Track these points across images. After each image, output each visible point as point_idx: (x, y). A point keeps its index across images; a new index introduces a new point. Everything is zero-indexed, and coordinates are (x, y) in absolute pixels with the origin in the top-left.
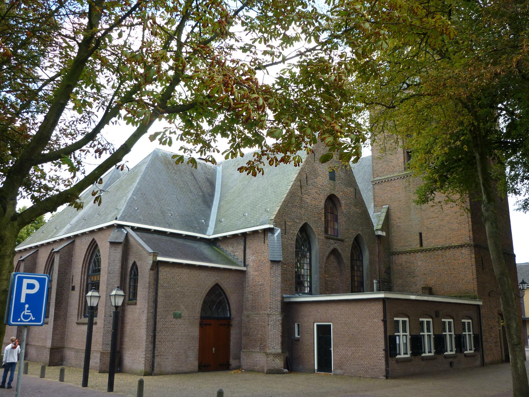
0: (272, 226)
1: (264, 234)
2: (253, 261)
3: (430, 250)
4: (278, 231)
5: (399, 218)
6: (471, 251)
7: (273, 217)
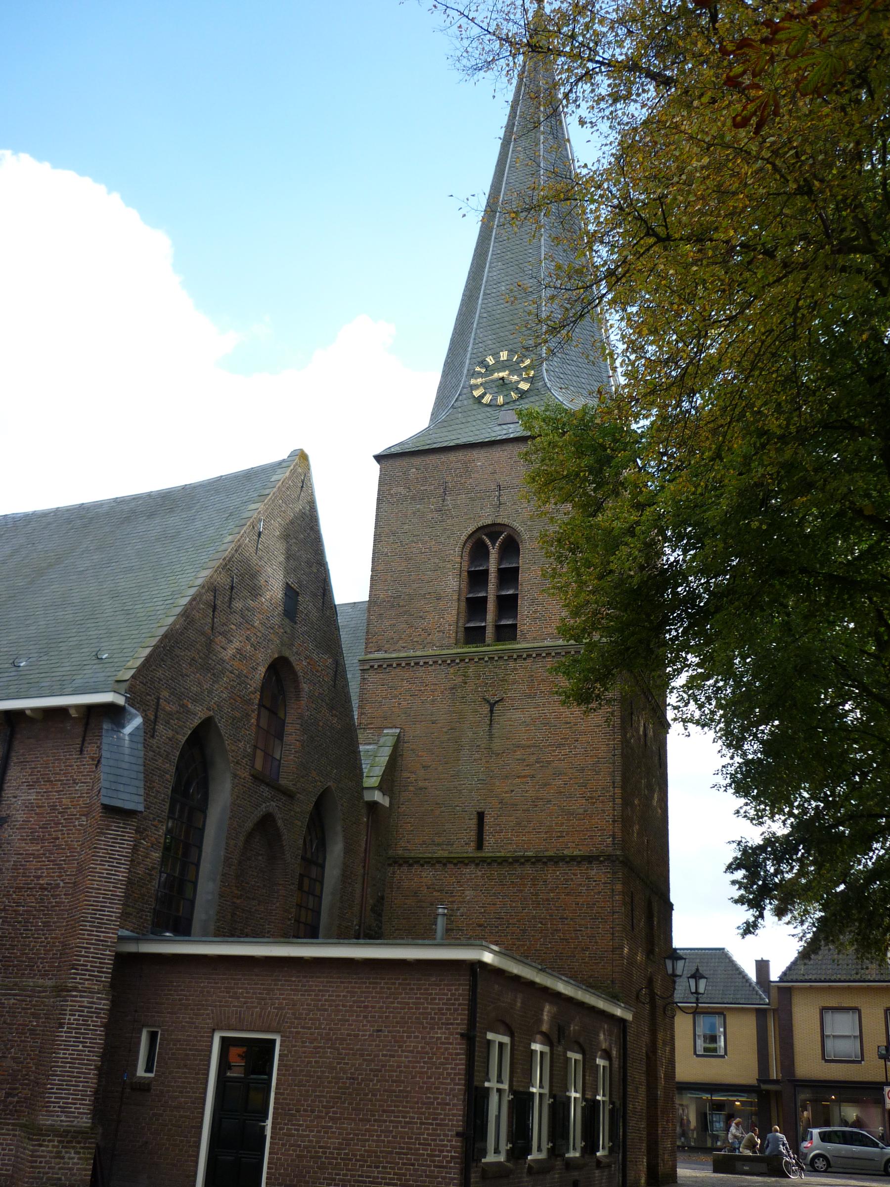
0: (120, 700)
1: (87, 725)
2: (29, 807)
3: (502, 861)
4: (136, 722)
5: (425, 767)
6: (614, 873)
7: (128, 675)
